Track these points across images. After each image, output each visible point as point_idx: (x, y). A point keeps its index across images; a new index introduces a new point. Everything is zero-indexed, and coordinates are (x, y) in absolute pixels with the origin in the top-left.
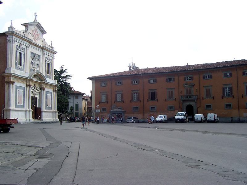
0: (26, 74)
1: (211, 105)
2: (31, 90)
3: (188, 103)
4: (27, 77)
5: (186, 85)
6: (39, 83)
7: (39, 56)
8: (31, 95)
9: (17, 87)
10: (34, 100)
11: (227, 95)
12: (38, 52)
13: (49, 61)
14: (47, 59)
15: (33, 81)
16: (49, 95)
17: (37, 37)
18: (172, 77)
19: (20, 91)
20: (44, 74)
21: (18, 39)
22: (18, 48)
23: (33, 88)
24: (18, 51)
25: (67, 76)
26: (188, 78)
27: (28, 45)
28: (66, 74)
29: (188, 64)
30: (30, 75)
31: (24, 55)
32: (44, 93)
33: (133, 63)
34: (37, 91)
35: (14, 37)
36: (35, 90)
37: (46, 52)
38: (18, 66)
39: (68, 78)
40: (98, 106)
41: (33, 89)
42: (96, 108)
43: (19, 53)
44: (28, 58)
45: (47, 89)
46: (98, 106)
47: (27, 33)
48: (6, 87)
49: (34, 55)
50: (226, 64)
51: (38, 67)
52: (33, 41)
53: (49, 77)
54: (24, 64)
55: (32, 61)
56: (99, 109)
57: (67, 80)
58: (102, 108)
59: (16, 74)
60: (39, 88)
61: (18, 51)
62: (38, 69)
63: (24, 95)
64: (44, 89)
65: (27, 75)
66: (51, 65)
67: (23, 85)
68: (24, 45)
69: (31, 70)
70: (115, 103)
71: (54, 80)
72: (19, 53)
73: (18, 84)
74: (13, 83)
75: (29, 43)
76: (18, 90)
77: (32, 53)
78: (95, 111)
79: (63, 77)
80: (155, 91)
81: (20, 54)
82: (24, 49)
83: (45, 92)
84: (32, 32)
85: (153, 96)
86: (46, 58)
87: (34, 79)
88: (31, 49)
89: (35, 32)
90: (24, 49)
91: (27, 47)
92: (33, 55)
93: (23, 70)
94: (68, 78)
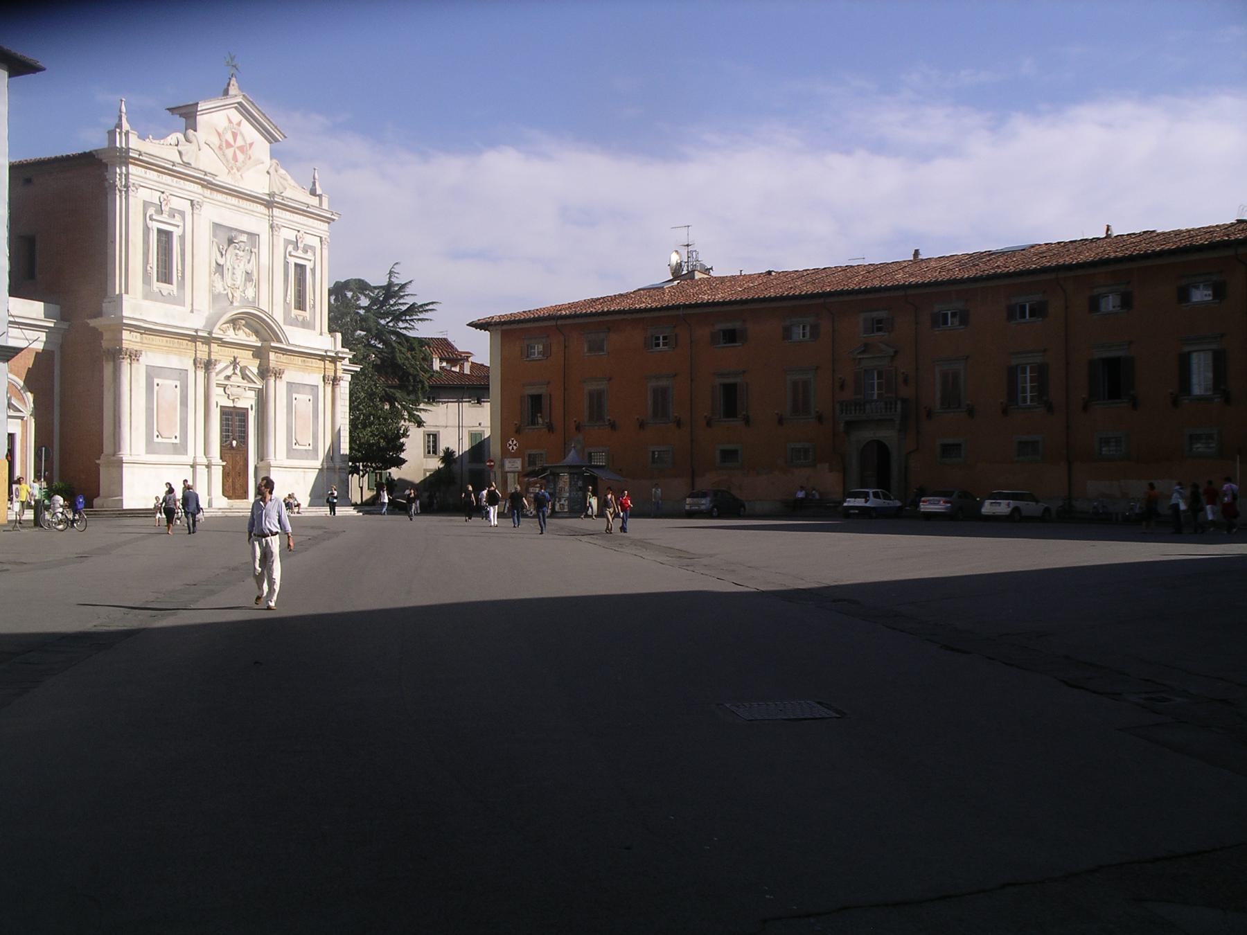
0: (193, 316)
1: (959, 445)
2: (216, 379)
3: (867, 435)
4: (196, 331)
5: (864, 352)
6: (259, 353)
7: (253, 236)
8: (220, 399)
9: (152, 373)
10: (233, 421)
11: (1025, 400)
12: (252, 220)
13: (300, 253)
14: (290, 248)
15: (223, 343)
16: (303, 399)
17: (240, 157)
18: (737, 325)
19: (168, 388)
20: (279, 315)
21: (152, 175)
22: (151, 211)
23: (229, 372)
24: (154, 226)
25: (412, 309)
26: (658, 338)
27: (196, 198)
28: (410, 301)
29: (917, 253)
30: (212, 322)
31: (182, 238)
32: (278, 391)
33: (690, 248)
34: (245, 383)
35: (132, 168)
36: (237, 379)
37: (288, 215)
38: (157, 286)
39: (421, 316)
40: (513, 445)
41: (228, 378)
42: (505, 453)
43: (159, 231)
44: (199, 251)
45: (290, 375)
46: (513, 445)
47: (193, 147)
48: (108, 369)
49: (229, 238)
50: (1058, 255)
51: (248, 284)
52: (224, 178)
53: (306, 325)
54: (183, 273)
55: (221, 261)
56: (514, 456)
57: (417, 325)
58: (529, 452)
59: (145, 321)
60: (255, 371)
61: (154, 226)
62: (250, 293)
63: (184, 403)
64: (278, 374)
65: (196, 322)
66: (313, 270)
67: (181, 359)
68: (180, 194)
69: (216, 298)
70: (709, 424)
71: (327, 336)
72: (159, 231)
73: (154, 356)
74: (134, 356)
75: (203, 186)
76: (156, 381)
77: (217, 226)
78: (502, 466)
79: (398, 316)
80: (738, 380)
81: (165, 236)
82: (182, 214)
83: (281, 386)
84: (215, 140)
85: (731, 400)
86: (287, 242)
87: (231, 335)
88: (218, 210)
89: (229, 137)
90: (182, 214)
91: (192, 205)
92: (223, 237)
93: (179, 301)
94: (421, 316)
